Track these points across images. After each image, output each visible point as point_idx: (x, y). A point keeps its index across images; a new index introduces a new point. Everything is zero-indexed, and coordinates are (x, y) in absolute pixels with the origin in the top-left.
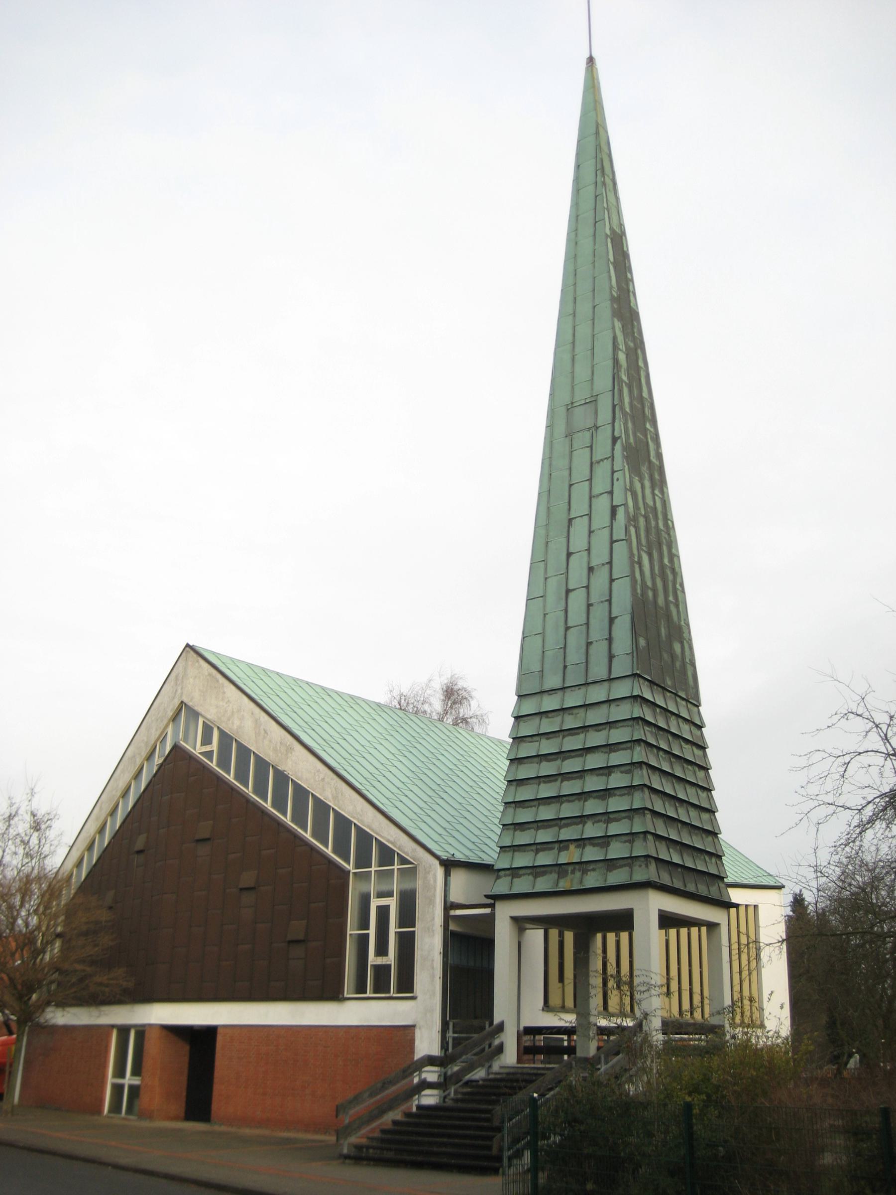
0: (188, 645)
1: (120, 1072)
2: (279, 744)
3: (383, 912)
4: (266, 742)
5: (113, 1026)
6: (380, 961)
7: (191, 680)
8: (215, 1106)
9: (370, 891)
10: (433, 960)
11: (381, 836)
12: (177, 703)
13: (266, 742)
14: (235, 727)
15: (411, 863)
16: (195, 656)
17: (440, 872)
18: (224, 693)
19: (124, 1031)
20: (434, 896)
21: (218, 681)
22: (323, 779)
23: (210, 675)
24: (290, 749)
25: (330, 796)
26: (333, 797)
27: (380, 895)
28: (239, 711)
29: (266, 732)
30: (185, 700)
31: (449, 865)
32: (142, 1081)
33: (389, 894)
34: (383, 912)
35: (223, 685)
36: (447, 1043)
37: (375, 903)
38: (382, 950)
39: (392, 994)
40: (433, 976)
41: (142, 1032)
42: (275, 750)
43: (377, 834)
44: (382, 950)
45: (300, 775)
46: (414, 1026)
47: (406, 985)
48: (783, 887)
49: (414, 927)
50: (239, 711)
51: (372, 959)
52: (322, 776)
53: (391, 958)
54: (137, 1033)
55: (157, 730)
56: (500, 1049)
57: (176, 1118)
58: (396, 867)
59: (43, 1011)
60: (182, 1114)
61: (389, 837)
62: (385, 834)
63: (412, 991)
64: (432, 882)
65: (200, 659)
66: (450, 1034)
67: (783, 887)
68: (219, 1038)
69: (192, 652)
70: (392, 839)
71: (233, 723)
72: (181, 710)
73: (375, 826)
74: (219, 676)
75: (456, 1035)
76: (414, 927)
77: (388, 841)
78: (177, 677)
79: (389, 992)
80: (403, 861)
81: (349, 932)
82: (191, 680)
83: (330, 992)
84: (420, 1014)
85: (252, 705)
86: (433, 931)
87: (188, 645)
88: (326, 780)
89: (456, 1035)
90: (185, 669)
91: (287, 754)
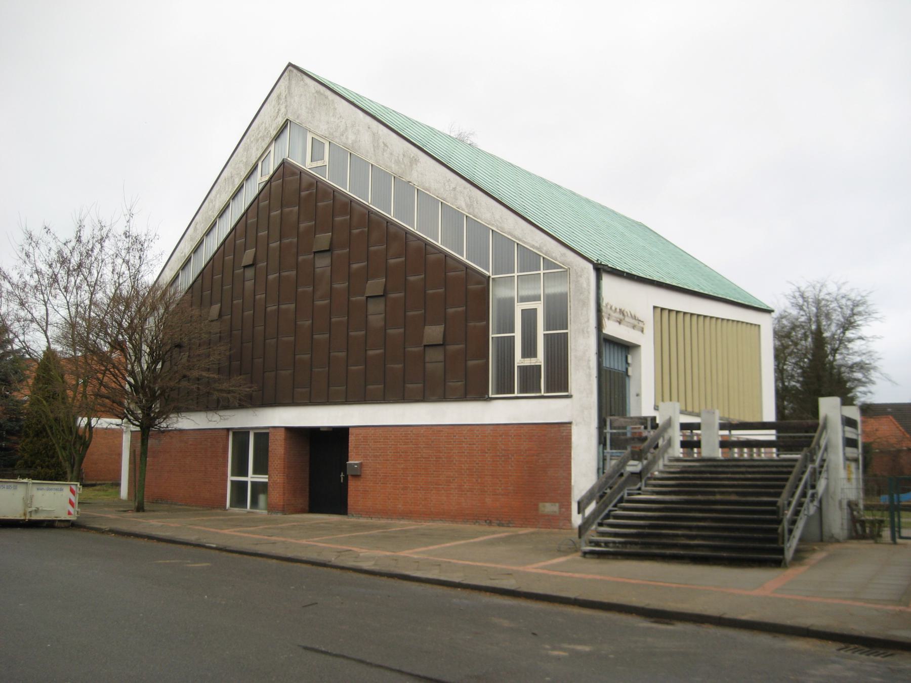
0: (290, 65)
1: (241, 469)
2: (401, 157)
3: (529, 317)
4: (386, 155)
5: (228, 430)
6: (528, 362)
7: (296, 99)
8: (351, 501)
9: (517, 297)
10: (589, 361)
11: (525, 242)
12: (280, 121)
13: (386, 155)
14: (350, 142)
15: (561, 267)
16: (299, 74)
17: (592, 275)
18: (335, 109)
19: (241, 435)
20: (588, 299)
21: (327, 97)
22: (454, 189)
23: (318, 92)
24: (414, 161)
25: (463, 205)
26: (467, 206)
27: (523, 299)
28: (353, 126)
29: (385, 145)
30: (291, 118)
31: (600, 269)
32: (269, 478)
33: (536, 298)
34: (529, 317)
35: (333, 101)
36: (605, 438)
37: (519, 308)
38: (529, 350)
39: (543, 393)
40: (590, 375)
41: (263, 436)
42: (397, 162)
43: (520, 240)
44: (529, 350)
45: (427, 185)
46: (570, 423)
47: (558, 383)
48: (773, 311)
49: (567, 329)
50: (353, 126)
51: (519, 360)
52: (453, 186)
53: (540, 359)
54: (257, 435)
55: (257, 149)
56: (669, 443)
57: (302, 511)
58: (542, 272)
59: (167, 417)
60: (307, 508)
61: (534, 243)
62: (529, 240)
63: (566, 389)
64: (585, 285)
65: (305, 77)
66: (608, 430)
67: (773, 311)
68: (352, 438)
69: (295, 71)
70: (536, 245)
71: (347, 138)
72: (286, 126)
73: (518, 233)
74: (328, 93)
75: (614, 431)
76: (567, 329)
77: (533, 246)
78: (279, 97)
79: (540, 391)
80: (549, 264)
81: (491, 336)
82: (296, 99)
83: (476, 392)
84: (576, 410)
85: (368, 119)
86: (588, 332)
87: (290, 65)
88: (458, 189)
89: (614, 431)
90: (289, 88)
91: (411, 166)
